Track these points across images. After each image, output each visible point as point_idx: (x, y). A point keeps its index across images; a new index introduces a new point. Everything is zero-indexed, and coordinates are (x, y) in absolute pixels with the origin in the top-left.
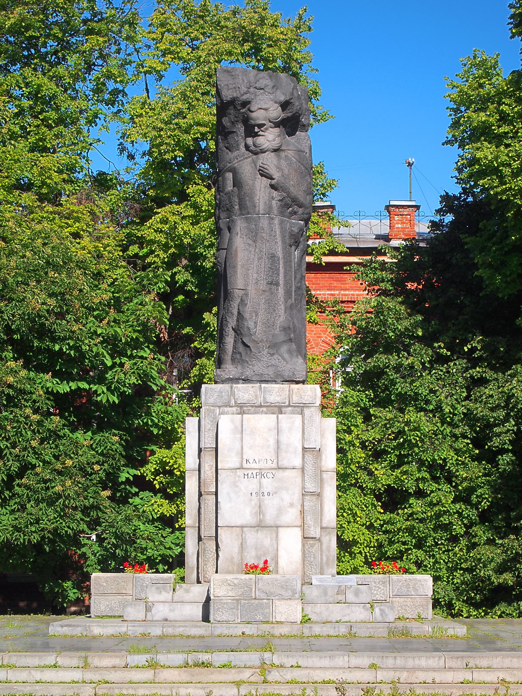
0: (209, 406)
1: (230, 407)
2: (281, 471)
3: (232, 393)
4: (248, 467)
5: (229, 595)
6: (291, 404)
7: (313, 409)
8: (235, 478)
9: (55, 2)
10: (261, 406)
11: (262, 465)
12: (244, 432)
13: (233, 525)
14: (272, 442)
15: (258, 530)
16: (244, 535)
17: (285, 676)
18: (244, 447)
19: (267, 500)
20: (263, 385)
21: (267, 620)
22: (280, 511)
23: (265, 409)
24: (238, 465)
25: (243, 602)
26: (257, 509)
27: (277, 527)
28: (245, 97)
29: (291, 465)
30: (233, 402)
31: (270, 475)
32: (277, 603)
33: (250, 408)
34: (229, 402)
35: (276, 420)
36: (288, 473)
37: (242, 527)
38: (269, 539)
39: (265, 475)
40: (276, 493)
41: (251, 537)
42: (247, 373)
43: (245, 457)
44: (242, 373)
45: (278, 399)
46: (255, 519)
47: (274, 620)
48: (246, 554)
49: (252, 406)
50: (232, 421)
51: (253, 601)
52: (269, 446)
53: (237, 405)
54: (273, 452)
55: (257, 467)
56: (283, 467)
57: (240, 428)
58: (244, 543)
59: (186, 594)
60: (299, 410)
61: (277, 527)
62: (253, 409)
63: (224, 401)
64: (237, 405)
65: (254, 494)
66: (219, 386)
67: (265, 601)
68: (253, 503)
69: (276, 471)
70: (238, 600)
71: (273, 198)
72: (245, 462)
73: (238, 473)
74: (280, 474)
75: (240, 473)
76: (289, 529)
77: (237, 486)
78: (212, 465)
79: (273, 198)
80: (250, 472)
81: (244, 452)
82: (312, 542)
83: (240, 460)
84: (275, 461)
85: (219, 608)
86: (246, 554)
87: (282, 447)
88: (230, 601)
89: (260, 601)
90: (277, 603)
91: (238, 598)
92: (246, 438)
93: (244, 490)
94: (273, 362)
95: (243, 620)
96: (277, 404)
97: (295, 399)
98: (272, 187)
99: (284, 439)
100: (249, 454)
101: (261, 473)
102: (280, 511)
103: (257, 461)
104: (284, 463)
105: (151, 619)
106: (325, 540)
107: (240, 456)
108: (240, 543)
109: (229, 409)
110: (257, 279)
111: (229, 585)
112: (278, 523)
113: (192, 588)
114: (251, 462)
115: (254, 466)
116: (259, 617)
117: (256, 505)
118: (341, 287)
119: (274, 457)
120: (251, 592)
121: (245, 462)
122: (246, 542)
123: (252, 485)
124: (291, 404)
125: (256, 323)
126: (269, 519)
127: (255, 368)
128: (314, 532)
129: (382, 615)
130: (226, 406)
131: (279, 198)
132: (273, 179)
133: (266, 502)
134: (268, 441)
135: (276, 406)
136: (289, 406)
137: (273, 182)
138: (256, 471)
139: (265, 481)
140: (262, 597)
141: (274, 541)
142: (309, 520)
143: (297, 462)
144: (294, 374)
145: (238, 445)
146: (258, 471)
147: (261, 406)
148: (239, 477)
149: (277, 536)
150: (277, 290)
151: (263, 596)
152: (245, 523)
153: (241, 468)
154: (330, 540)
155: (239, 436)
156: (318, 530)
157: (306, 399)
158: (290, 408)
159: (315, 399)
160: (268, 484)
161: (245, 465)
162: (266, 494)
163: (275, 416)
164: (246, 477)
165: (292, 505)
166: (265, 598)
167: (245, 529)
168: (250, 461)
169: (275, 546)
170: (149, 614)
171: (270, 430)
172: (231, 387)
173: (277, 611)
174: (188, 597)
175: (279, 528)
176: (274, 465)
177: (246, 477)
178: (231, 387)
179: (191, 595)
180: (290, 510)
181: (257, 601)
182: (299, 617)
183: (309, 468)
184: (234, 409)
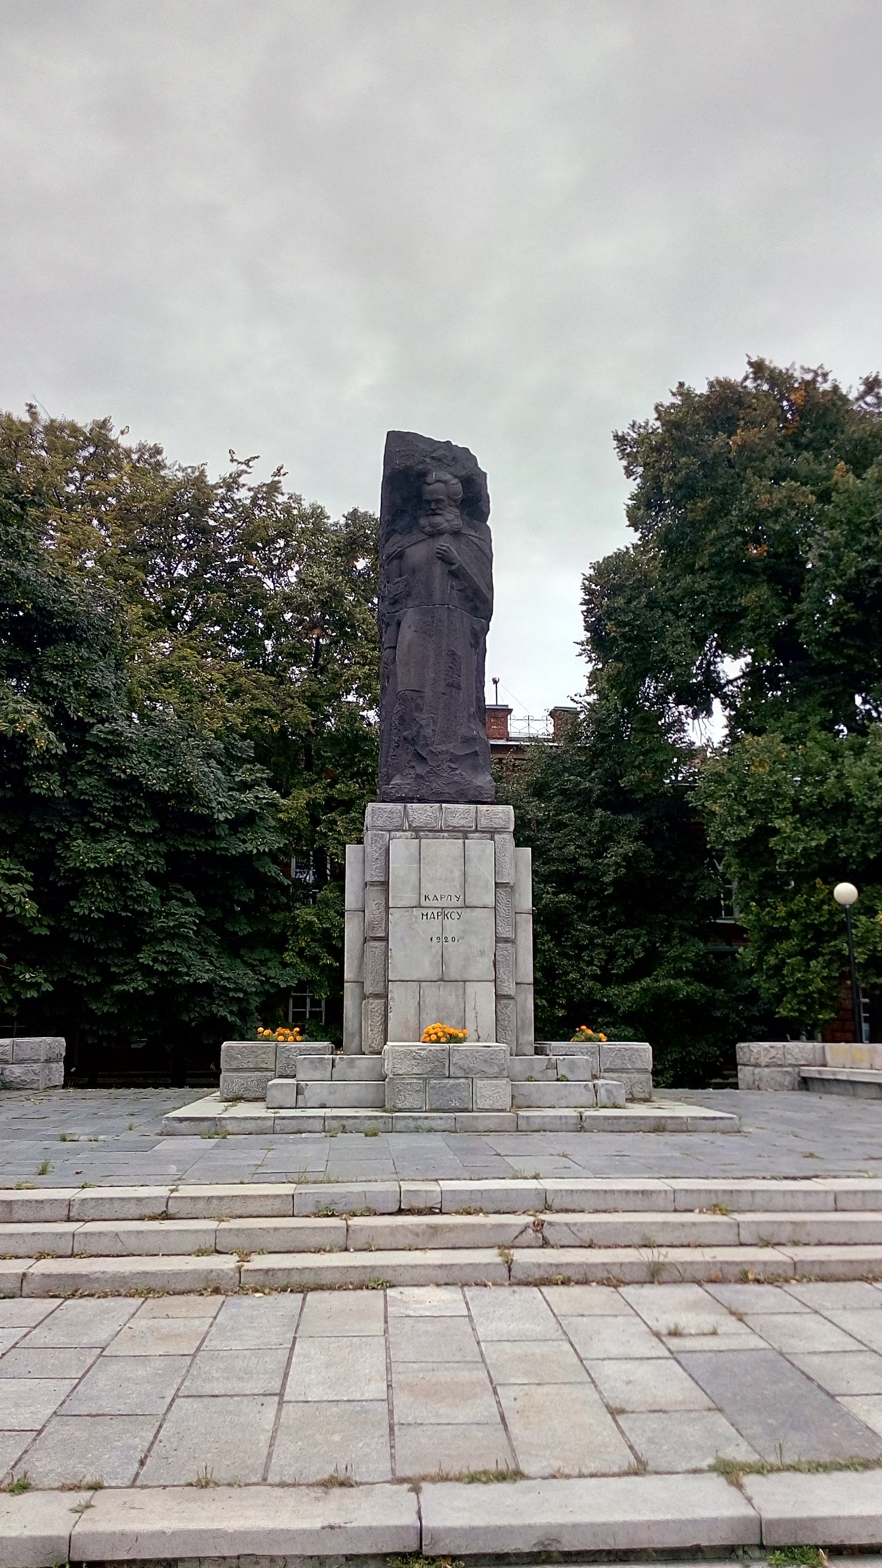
0: (377, 830)
1: (404, 831)
2: (468, 910)
4: (427, 905)
5: (414, 1072)
7: (505, 836)
10: (441, 831)
14: (457, 874)
17: (579, 1234)
20: (444, 805)
21: (466, 1106)
23: (446, 834)
25: (433, 1082)
27: (464, 981)
28: (420, 467)
31: (456, 916)
32: (479, 1083)
34: (402, 825)
38: (454, 997)
40: (463, 938)
41: (432, 994)
43: (423, 893)
45: (463, 822)
48: (424, 1016)
49: (429, 831)
51: (446, 1081)
53: (411, 828)
54: (458, 886)
59: (349, 1070)
60: (489, 836)
62: (431, 834)
64: (411, 828)
65: (434, 940)
66: (390, 806)
67: (462, 1080)
69: (462, 910)
72: (423, 898)
73: (415, 913)
74: (467, 914)
80: (430, 911)
82: (505, 1001)
85: (400, 1091)
86: (424, 1016)
87: (470, 879)
88: (415, 1081)
89: (457, 1081)
90: (479, 1083)
94: (455, 778)
95: (434, 1107)
97: (483, 823)
98: (451, 573)
101: (444, 913)
105: (303, 1105)
106: (520, 999)
107: (417, 891)
108: (417, 1003)
109: (402, 833)
111: (414, 1059)
112: (466, 977)
116: (455, 1104)
117: (437, 952)
118: (228, 982)
119: (460, 894)
120: (444, 1067)
121: (423, 898)
122: (424, 1001)
123: (434, 927)
126: (453, 972)
128: (509, 988)
129: (609, 1097)
130: (398, 830)
131: (459, 587)
132: (453, 564)
134: (452, 872)
136: (476, 831)
137: (453, 567)
141: (461, 1000)
142: (503, 974)
143: (490, 900)
145: (414, 878)
146: (440, 910)
148: (416, 917)
151: (459, 1073)
154: (526, 999)
155: (416, 866)
156: (513, 986)
157: (498, 823)
158: (477, 834)
159: (508, 823)
160: (452, 926)
161: (424, 903)
162: (450, 939)
163: (461, 841)
164: (425, 917)
165: (482, 953)
168: (431, 897)
170: (300, 1097)
173: (478, 1094)
174: (351, 1073)
175: (467, 983)
176: (460, 903)
177: (425, 917)
178: (405, 807)
179: (356, 1070)
180: (479, 959)
181: (452, 1081)
183: (501, 909)
184: (408, 834)
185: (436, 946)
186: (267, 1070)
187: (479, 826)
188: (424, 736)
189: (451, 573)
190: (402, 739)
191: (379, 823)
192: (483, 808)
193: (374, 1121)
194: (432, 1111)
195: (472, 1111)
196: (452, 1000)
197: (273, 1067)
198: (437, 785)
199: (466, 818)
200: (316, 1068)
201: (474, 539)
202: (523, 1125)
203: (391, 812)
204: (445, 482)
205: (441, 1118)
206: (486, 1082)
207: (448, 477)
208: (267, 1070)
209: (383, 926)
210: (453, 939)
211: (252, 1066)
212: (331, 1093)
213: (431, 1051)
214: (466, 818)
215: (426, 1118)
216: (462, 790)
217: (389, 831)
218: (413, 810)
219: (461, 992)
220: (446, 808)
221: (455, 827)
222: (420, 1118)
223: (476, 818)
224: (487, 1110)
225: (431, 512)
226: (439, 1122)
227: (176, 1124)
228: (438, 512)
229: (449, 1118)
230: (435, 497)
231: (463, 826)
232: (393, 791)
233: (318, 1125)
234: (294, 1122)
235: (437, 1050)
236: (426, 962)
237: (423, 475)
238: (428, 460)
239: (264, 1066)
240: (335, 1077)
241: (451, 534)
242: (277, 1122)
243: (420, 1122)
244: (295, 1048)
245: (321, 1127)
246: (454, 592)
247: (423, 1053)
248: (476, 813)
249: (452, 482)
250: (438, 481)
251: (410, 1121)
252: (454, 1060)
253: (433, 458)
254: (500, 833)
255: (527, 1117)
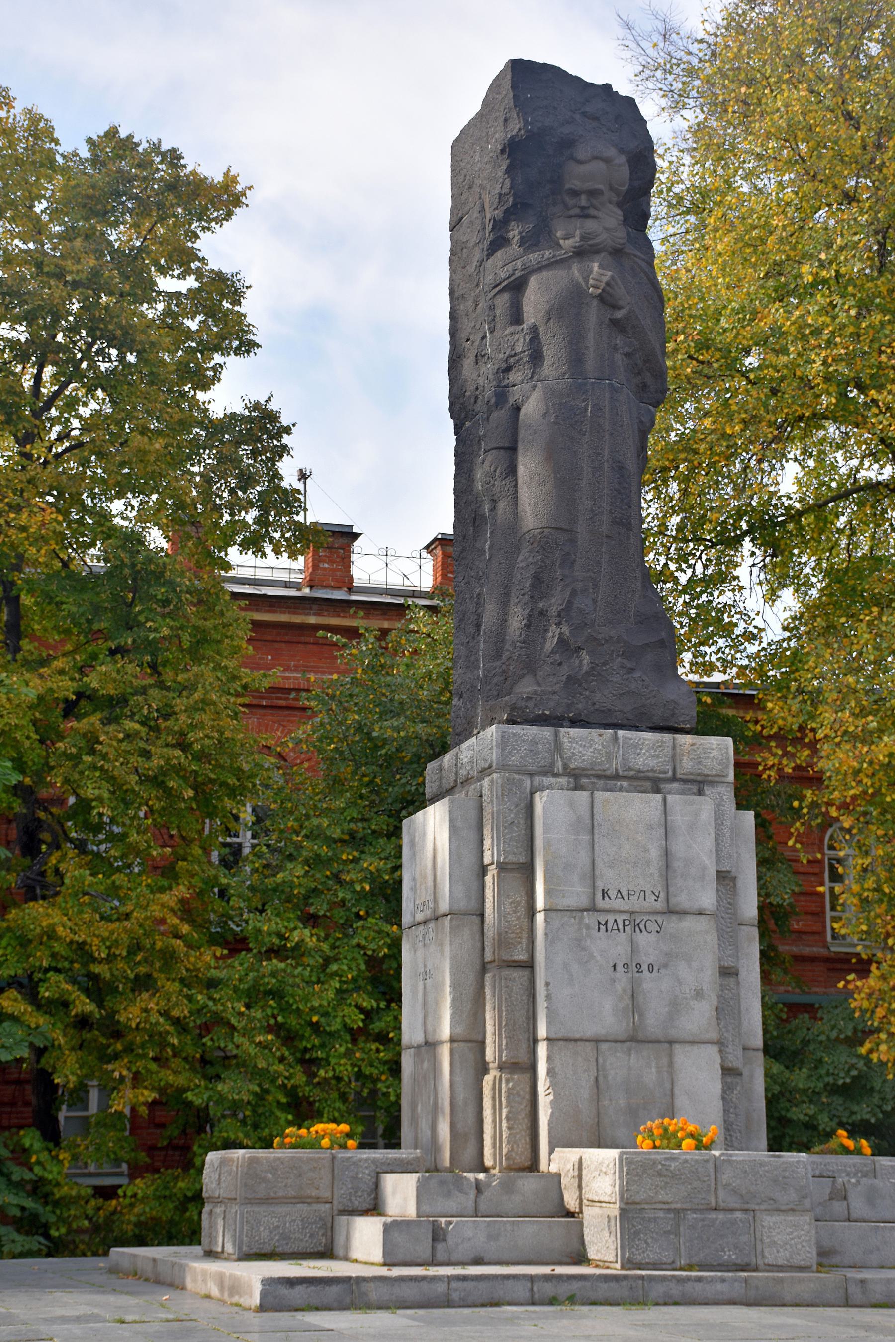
1: (556, 775)
2: (674, 917)
3: (557, 745)
6: (679, 776)
8: (580, 929)
9: (4, 167)
10: (616, 777)
11: (635, 903)
12: (596, 831)
13: (577, 1036)
14: (655, 853)
15: (630, 1050)
16: (601, 1060)
18: (598, 861)
19: (648, 981)
20: (621, 733)
21: (746, 1260)
22: (675, 1006)
23: (625, 784)
24: (584, 902)
25: (692, 1216)
26: (627, 1000)
27: (671, 1043)
28: (566, 130)
29: (695, 906)
30: (559, 765)
32: (769, 1220)
33: (594, 780)
34: (553, 764)
35: (660, 807)
36: (689, 923)
37: (597, 1041)
38: (654, 1070)
39: (642, 926)
40: (666, 966)
42: (580, 706)
43: (600, 885)
44: (569, 706)
45: (652, 763)
46: (624, 1025)
47: (760, 1262)
48: (606, 1103)
50: (571, 804)
51: (713, 1215)
52: (648, 863)
53: (568, 772)
54: (656, 875)
55: (627, 908)
56: (677, 909)
57: (588, 821)
58: (601, 1079)
60: (695, 788)
61: (671, 1043)
63: (543, 763)
64: (568, 772)
65: (620, 968)
68: (619, 987)
69: (664, 917)
70: (677, 1211)
71: (615, 348)
72: (599, 895)
73: (586, 921)
74: (673, 925)
75: (589, 919)
76: (695, 1048)
77: (584, 949)
78: (519, 903)
79: (615, 348)
80: (611, 918)
81: (597, 873)
83: (590, 890)
84: (662, 895)
86: (606, 1103)
87: (677, 864)
88: (661, 1214)
91: (679, 1206)
92: (602, 842)
93: (599, 958)
94: (633, 686)
95: (695, 1260)
96: (650, 775)
97: (687, 766)
99: (678, 847)
100: (608, 878)
102: (675, 1006)
103: (625, 893)
104: (682, 900)
108: (592, 1079)
110: (592, 511)
112: (673, 1033)
113: (520, 1183)
114: (613, 897)
115: (618, 904)
116: (730, 1256)
117: (624, 991)
119: (659, 888)
122: (605, 1077)
124: (679, 776)
125: (595, 601)
126: (653, 1023)
127: (598, 697)
128: (736, 1059)
130: (545, 774)
131: (627, 349)
133: (645, 985)
134: (646, 851)
135: (648, 779)
136: (674, 779)
137: (619, 314)
138: (624, 916)
139: (643, 939)
140: (732, 1205)
144: (673, 715)
145: (583, 858)
147: (616, 777)
148: (588, 927)
149: (671, 1064)
150: (629, 538)
151: (733, 1202)
152: (603, 1032)
153: (593, 908)
155: (586, 837)
157: (710, 767)
161: (601, 903)
162: (645, 967)
164: (603, 928)
165: (699, 994)
166: (737, 1206)
167: (604, 1046)
168: (613, 893)
169: (668, 1085)
170: (440, 1246)
171: (650, 827)
172: (556, 734)
173: (766, 1240)
175: (677, 1048)
176: (660, 905)
177: (603, 928)
180: (695, 1004)
181: (721, 1216)
182: (808, 1254)
184: (563, 781)
185: (622, 980)
186: (318, 1200)
187: (679, 771)
188: (581, 611)
189: (614, 322)
190: (536, 613)
191: (514, 760)
192: (685, 740)
193: (613, 1285)
194: (690, 1268)
195: (756, 1270)
196: (650, 1076)
197: (327, 1194)
198: (604, 697)
199: (658, 756)
200: (448, 1195)
201: (640, 262)
202: (855, 1292)
203: (534, 742)
204: (607, 160)
205: (723, 1280)
206: (776, 1218)
207: (612, 152)
208: (318, 1200)
209: (524, 941)
210: (651, 969)
211: (292, 1193)
212: (491, 1237)
213: (686, 1161)
214: (658, 756)
215: (699, 1280)
216: (644, 706)
217: (531, 775)
218: (572, 740)
219: (665, 1061)
220: (625, 738)
221: (639, 771)
222: (688, 1279)
223: (674, 757)
224: (780, 1268)
225: (577, 211)
226: (719, 1287)
227: (284, 1291)
228: (592, 212)
229: (735, 1280)
230: (589, 185)
231: (652, 771)
232: (531, 704)
233: (522, 1291)
234: (482, 1285)
235: (696, 1161)
236: (608, 1006)
237: (567, 144)
238: (577, 117)
239: (314, 1193)
240: (483, 1207)
241: (610, 254)
242: (454, 1285)
243: (689, 1287)
244: (367, 1160)
245: (527, 1294)
246: (618, 357)
247: (673, 1165)
248: (674, 747)
249: (617, 161)
250: (596, 158)
251: (672, 1285)
252: (725, 1178)
253: (584, 114)
254: (712, 783)
255: (863, 1282)
